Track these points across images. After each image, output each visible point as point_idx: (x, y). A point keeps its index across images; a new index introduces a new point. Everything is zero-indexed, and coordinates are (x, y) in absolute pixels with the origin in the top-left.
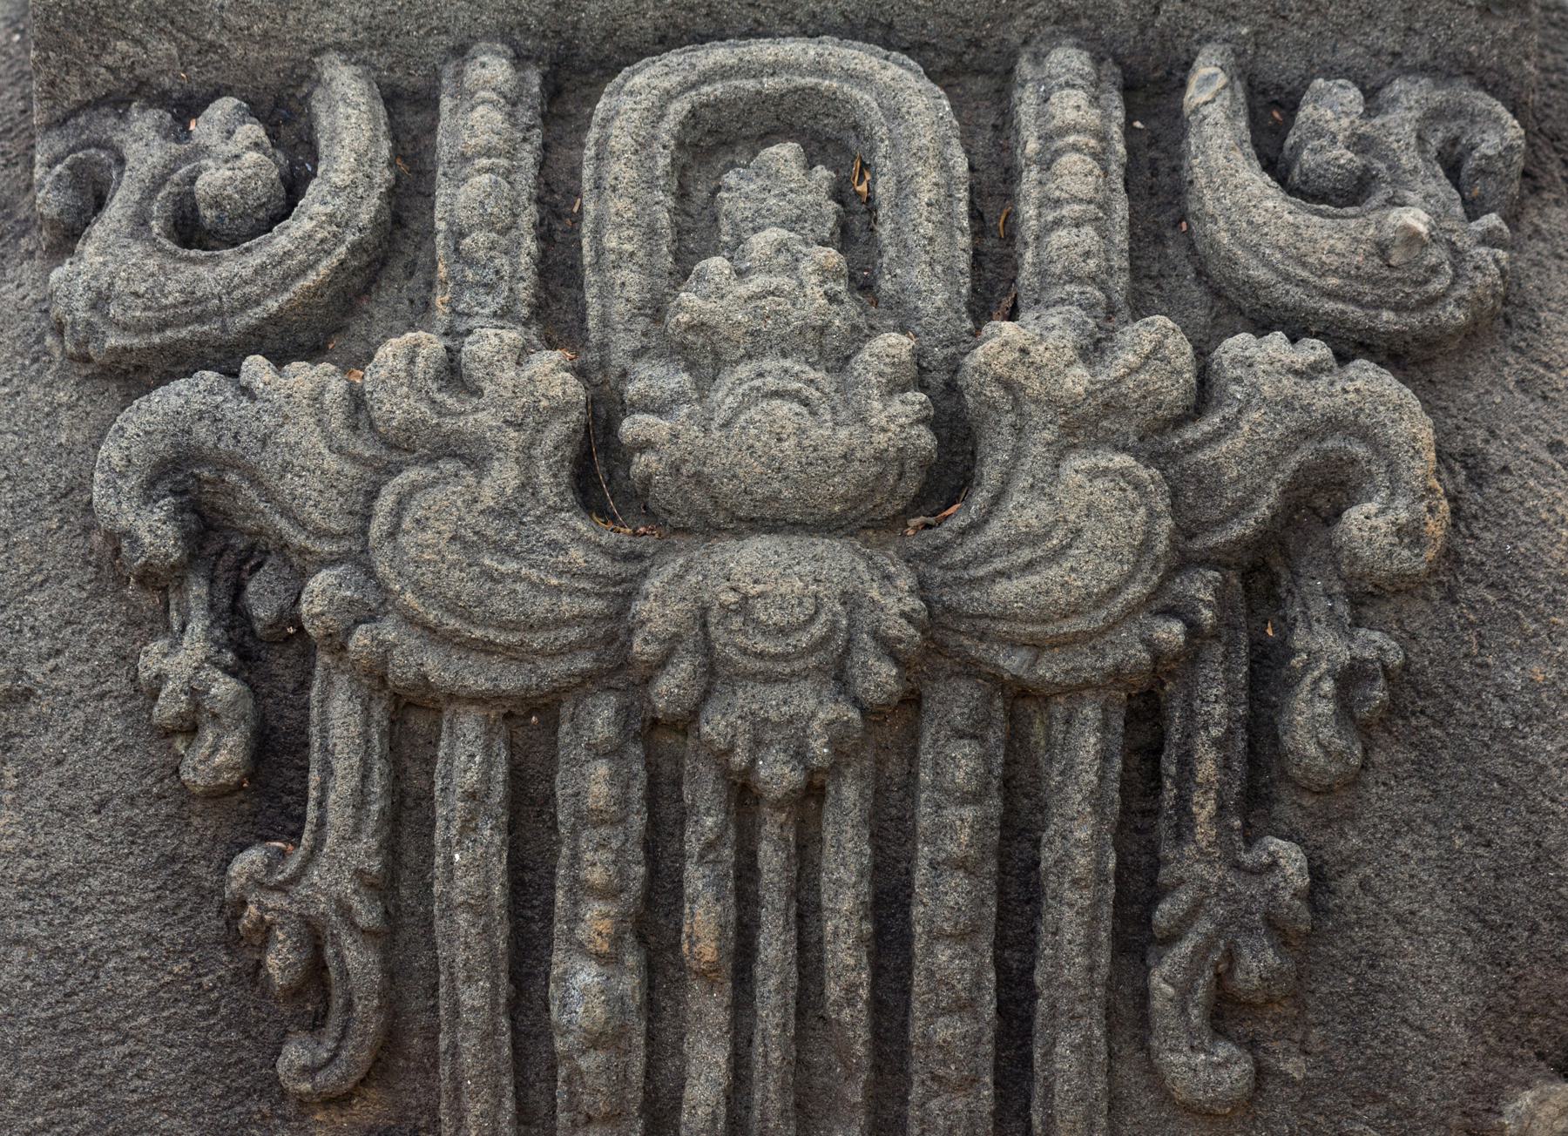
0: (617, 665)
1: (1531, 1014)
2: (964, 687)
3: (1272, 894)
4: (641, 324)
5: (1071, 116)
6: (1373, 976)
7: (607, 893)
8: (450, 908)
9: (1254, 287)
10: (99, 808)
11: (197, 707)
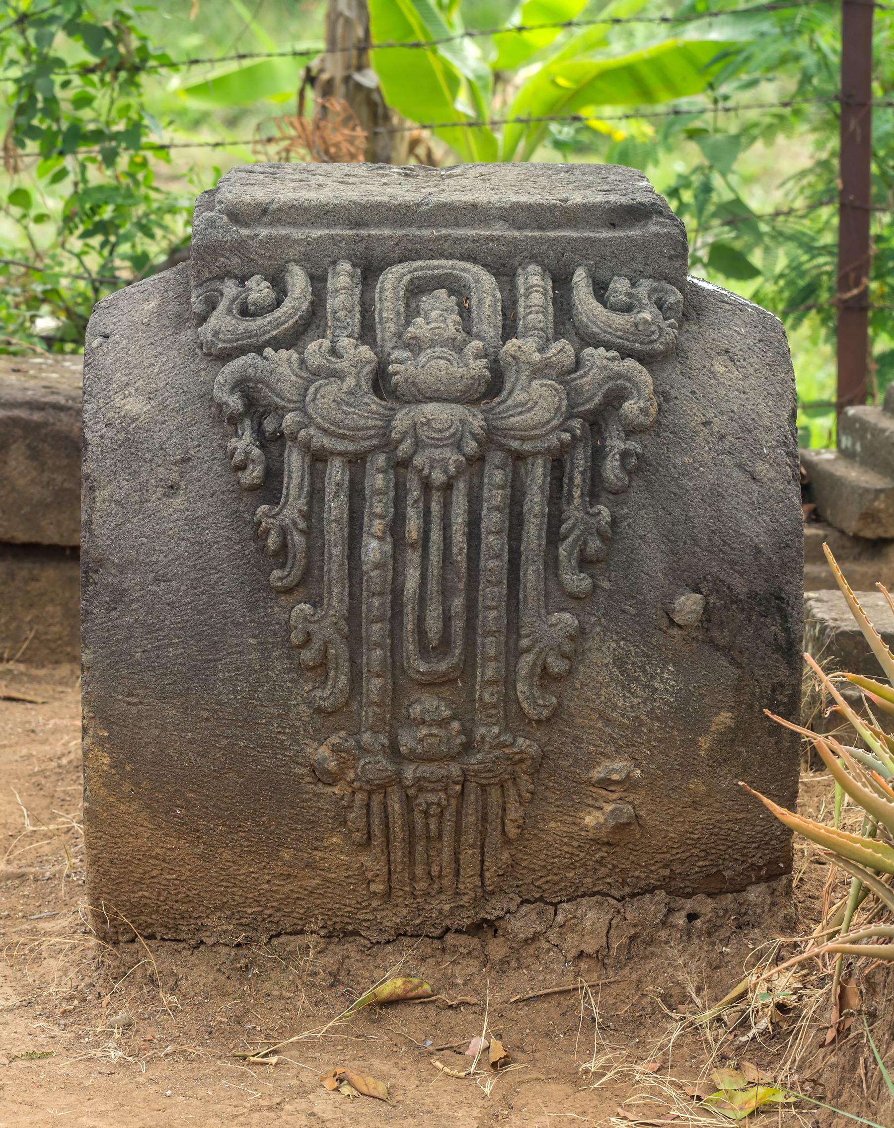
0: (387, 444)
1: (684, 571)
2: (499, 453)
3: (599, 522)
4: (395, 339)
5: (535, 282)
6: (632, 556)
7: (381, 517)
8: (330, 522)
9: (595, 334)
10: (212, 495)
11: (247, 458)
